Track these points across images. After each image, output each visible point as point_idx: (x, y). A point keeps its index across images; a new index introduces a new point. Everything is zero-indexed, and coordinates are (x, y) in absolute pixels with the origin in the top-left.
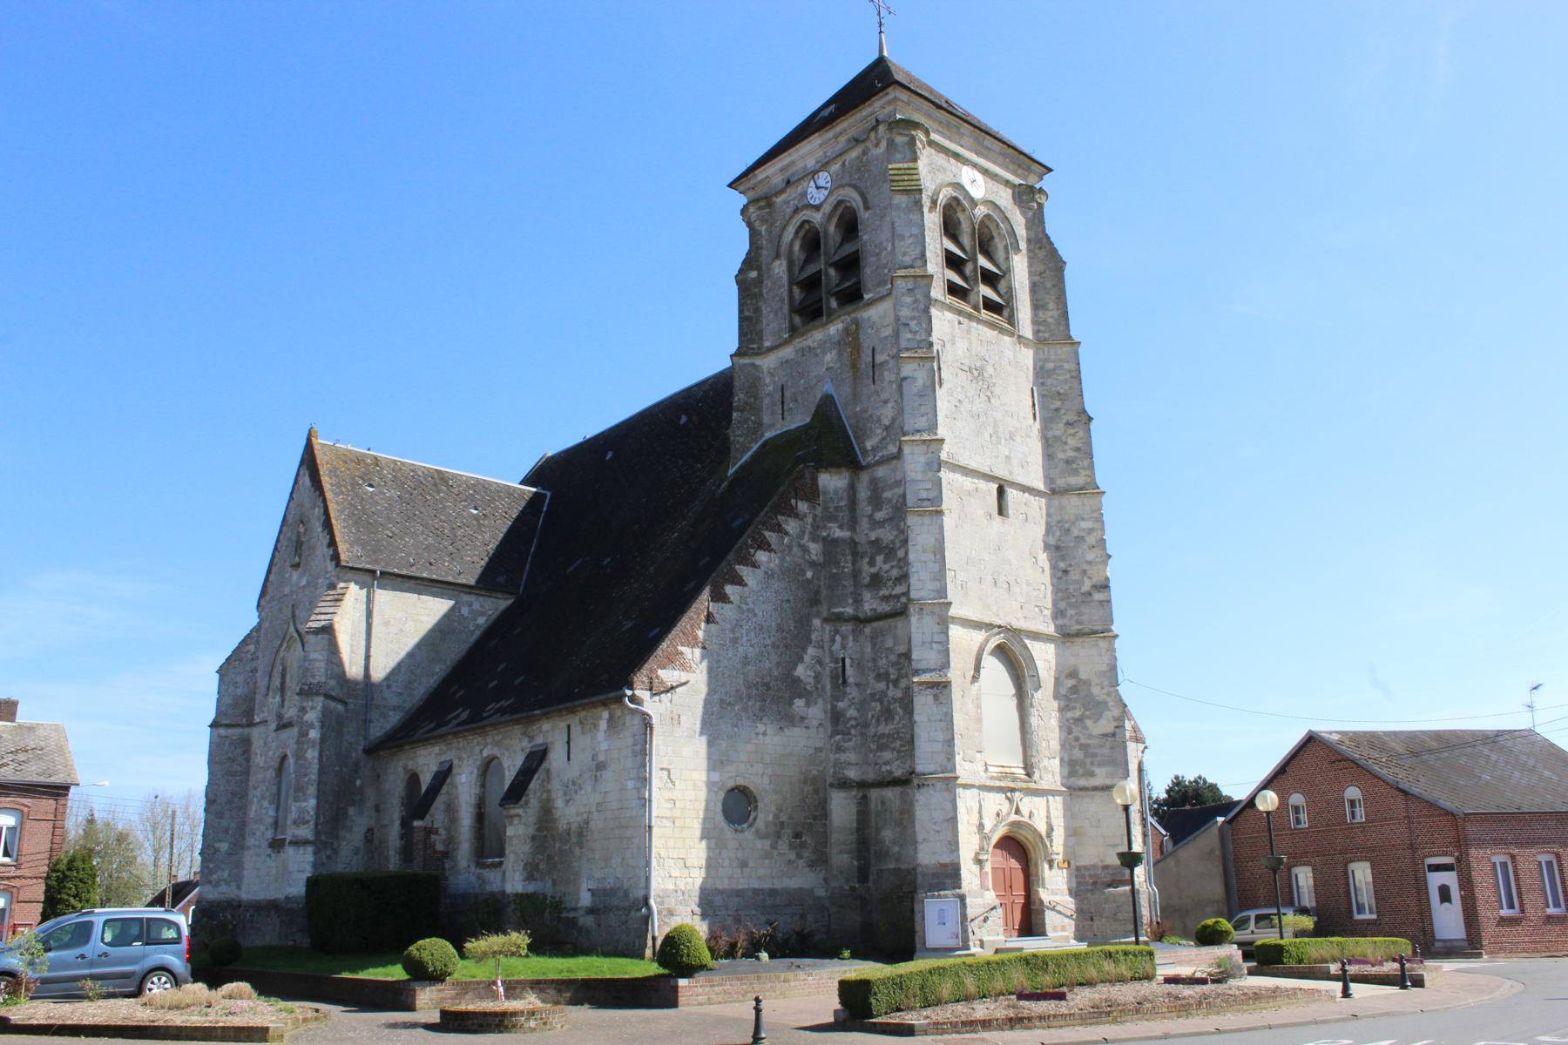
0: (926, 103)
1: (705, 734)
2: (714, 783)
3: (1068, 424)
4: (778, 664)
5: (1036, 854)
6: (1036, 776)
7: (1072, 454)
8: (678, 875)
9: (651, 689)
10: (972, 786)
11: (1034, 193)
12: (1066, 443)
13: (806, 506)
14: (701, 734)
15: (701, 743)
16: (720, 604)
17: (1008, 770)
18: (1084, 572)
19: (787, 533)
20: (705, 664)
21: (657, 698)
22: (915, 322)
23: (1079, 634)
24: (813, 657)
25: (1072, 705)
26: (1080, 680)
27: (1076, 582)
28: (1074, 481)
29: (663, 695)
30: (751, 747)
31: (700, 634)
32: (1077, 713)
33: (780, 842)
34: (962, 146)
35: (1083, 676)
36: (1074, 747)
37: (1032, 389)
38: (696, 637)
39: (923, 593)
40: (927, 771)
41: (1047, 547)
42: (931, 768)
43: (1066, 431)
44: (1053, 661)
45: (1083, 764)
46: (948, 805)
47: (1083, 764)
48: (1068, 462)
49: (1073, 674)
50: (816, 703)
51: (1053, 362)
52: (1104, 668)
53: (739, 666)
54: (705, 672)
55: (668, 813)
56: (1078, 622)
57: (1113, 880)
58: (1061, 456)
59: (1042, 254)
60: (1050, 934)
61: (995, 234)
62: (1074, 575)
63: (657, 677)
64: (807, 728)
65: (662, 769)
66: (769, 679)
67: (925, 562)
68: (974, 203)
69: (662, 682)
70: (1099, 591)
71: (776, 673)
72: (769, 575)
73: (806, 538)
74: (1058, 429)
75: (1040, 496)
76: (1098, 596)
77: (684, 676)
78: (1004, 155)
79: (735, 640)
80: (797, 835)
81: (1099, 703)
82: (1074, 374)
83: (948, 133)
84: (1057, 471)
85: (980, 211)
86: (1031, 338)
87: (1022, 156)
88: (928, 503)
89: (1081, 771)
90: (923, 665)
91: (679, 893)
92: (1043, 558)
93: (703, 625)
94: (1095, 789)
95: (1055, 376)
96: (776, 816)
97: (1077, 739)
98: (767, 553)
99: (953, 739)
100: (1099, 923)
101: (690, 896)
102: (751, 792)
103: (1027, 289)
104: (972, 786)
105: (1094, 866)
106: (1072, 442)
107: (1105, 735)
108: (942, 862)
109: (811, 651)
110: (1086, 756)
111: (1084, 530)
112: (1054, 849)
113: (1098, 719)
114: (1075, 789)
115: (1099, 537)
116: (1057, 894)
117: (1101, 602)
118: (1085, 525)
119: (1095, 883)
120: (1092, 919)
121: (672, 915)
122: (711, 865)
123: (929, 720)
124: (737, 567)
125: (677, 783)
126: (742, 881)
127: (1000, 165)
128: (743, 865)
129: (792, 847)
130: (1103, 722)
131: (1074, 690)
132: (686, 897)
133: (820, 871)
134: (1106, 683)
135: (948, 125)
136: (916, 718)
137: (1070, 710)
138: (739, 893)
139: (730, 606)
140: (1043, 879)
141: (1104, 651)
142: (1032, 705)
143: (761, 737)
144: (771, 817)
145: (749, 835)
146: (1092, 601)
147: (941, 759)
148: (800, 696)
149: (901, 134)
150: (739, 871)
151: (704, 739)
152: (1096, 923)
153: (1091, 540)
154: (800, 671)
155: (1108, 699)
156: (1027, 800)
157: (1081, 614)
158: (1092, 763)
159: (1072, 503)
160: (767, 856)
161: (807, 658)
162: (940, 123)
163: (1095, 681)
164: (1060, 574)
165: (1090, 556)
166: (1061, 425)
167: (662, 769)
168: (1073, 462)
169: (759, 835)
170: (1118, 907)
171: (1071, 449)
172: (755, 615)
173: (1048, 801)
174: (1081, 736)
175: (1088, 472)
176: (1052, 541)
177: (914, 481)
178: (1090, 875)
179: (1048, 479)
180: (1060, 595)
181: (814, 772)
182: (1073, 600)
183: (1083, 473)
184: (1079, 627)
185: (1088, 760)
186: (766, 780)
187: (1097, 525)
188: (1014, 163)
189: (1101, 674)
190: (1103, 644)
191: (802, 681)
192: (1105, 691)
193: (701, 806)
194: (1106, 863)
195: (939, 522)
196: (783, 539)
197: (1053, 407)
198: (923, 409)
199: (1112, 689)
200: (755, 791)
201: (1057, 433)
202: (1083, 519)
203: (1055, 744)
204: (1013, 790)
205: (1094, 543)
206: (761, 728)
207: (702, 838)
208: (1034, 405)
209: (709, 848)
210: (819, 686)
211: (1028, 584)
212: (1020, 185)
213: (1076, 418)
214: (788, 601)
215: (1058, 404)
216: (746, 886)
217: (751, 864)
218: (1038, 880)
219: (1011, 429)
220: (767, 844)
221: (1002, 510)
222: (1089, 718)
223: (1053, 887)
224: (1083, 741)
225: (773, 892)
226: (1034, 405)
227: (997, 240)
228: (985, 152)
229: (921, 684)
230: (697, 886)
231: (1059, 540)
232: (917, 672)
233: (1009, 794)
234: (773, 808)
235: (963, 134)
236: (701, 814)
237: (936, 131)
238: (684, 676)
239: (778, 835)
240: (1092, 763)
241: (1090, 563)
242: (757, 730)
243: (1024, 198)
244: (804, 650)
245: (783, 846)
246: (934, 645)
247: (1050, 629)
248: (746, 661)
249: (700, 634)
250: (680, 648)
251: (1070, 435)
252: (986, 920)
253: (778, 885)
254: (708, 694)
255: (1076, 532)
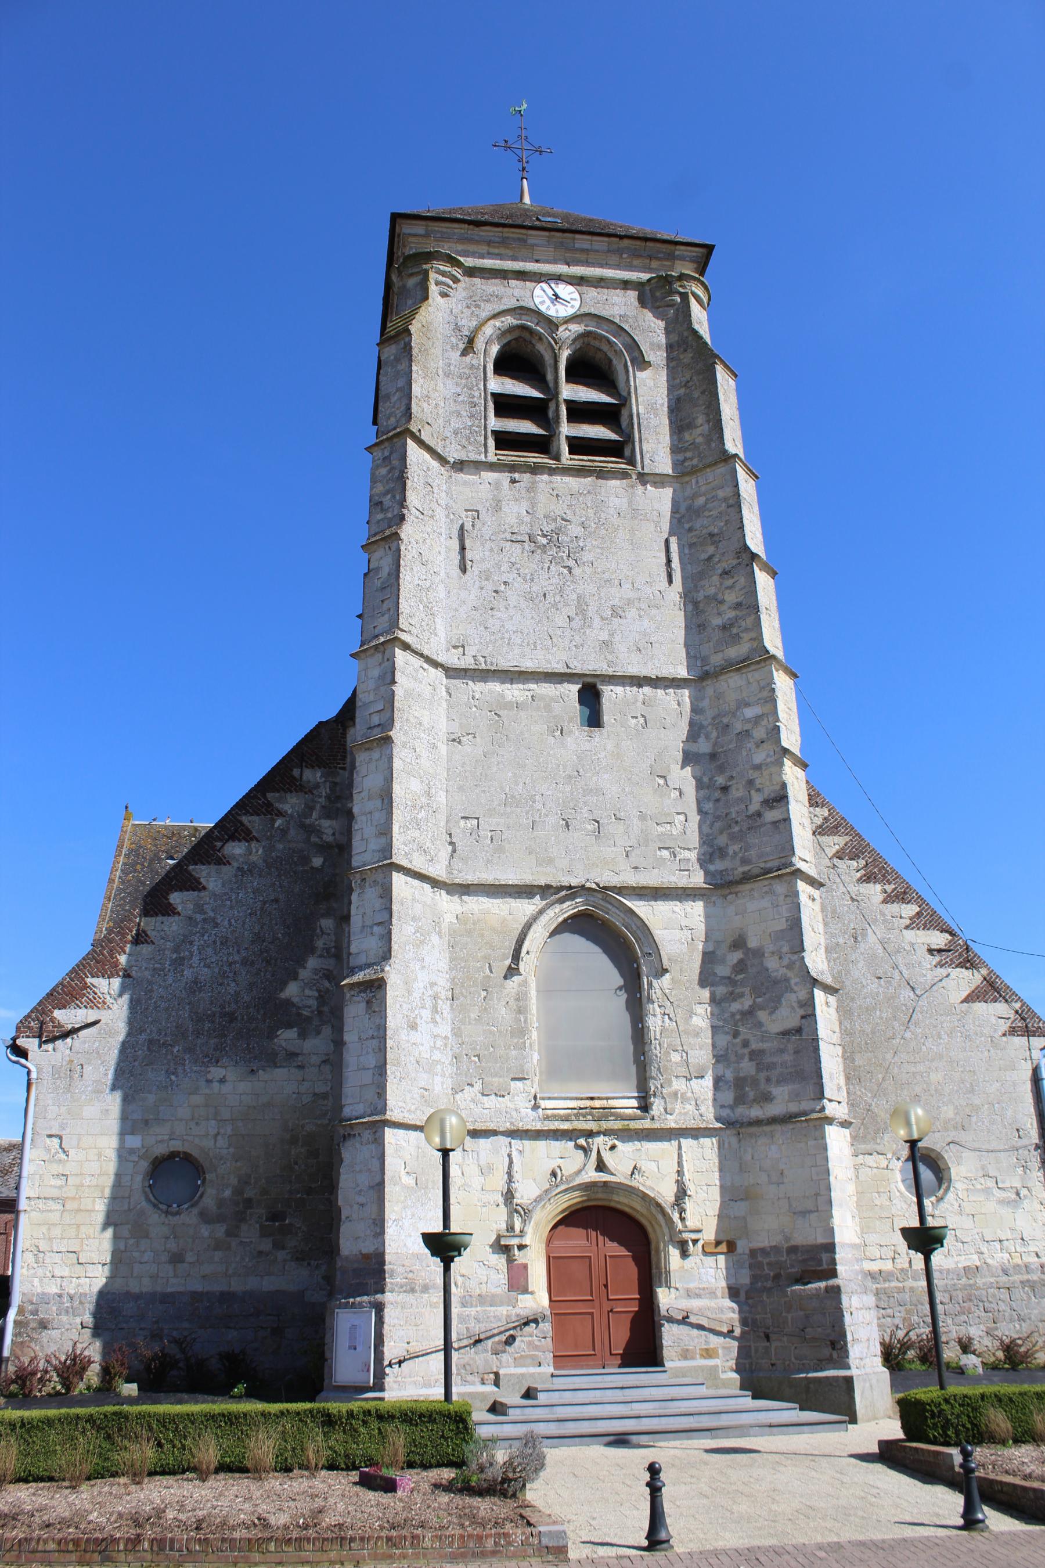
0: (456, 225)
1: (121, 1088)
2: (132, 1151)
3: (726, 573)
4: (251, 986)
5: (658, 1233)
6: (657, 1106)
7: (731, 614)
8: (66, 1273)
9: (40, 1037)
10: (495, 1133)
11: (670, 284)
12: (722, 602)
13: (319, 774)
14: (114, 1088)
15: (114, 1102)
16: (160, 918)
17: (597, 1104)
18: (751, 782)
19: (280, 814)
20: (126, 997)
21: (50, 1047)
22: (389, 496)
23: (747, 878)
24: (316, 971)
25: (738, 990)
26: (748, 951)
27: (740, 800)
28: (734, 652)
29: (59, 1043)
30: (197, 1099)
31: (123, 959)
32: (747, 1003)
33: (244, 1227)
34: (537, 261)
35: (753, 943)
36: (742, 1057)
37: (667, 542)
38: (116, 964)
39: (367, 857)
40: (355, 1114)
41: (688, 758)
42: (360, 1109)
43: (721, 584)
44: (702, 927)
45: (755, 1082)
46: (376, 1163)
47: (755, 1082)
48: (724, 628)
49: (739, 943)
50: (318, 1033)
51: (704, 495)
52: (782, 925)
53: (184, 994)
54: (126, 1007)
55: (55, 1193)
56: (744, 861)
57: (804, 1272)
58: (717, 621)
59: (687, 358)
60: (668, 1364)
61: (611, 355)
62: (737, 792)
63: (53, 1020)
64: (301, 1067)
65: (50, 1136)
66: (234, 1006)
67: (370, 813)
68: (552, 324)
69: (60, 1026)
70: (772, 808)
71: (247, 998)
72: (246, 871)
73: (315, 815)
74: (711, 586)
75: (678, 687)
76: (771, 816)
77: (91, 1015)
78: (619, 252)
79: (179, 962)
80: (274, 1217)
81: (776, 982)
82: (731, 502)
83: (510, 253)
84: (711, 644)
85: (568, 333)
86: (670, 472)
87: (649, 244)
88: (379, 729)
89: (751, 1095)
90: (362, 960)
91: (65, 1299)
92: (684, 778)
93: (128, 948)
94: (773, 1121)
95: (706, 514)
96: (238, 1191)
97: (746, 1044)
98: (244, 845)
99: (385, 1063)
100: (778, 1344)
101: (81, 1303)
102: (196, 1159)
103: (666, 409)
104: (495, 1133)
105: (776, 1249)
106: (731, 598)
107: (785, 1033)
108: (364, 1251)
109: (312, 963)
110: (759, 1070)
111: (749, 721)
112: (690, 1223)
113: (776, 1008)
114: (742, 1125)
115: (771, 726)
116: (698, 1296)
117: (775, 823)
118: (749, 712)
119: (777, 1277)
120: (767, 1337)
121: (45, 1328)
122: (119, 1260)
123: (360, 1039)
124: (191, 867)
125: (72, 1152)
126: (173, 1281)
127: (618, 267)
128: (177, 1259)
129: (264, 1232)
130: (783, 1012)
131: (740, 967)
132: (76, 1303)
133: (317, 1267)
134: (785, 949)
135: (504, 242)
136: (347, 1037)
137: (734, 1000)
138: (166, 1298)
139: (176, 918)
140: (668, 1273)
141: (782, 898)
142: (650, 1000)
143: (216, 1085)
144: (228, 1193)
145: (189, 1218)
146: (763, 825)
147: (370, 1094)
148: (289, 1026)
149: (412, 275)
150: (170, 1268)
151: (118, 1096)
152: (775, 1344)
153: (759, 733)
154: (292, 990)
155: (790, 974)
156: (625, 1148)
157: (747, 848)
158: (768, 1080)
159: (733, 684)
160: (218, 1246)
161: (304, 974)
162: (489, 243)
163: (769, 948)
164: (717, 794)
165: (759, 758)
166: (716, 579)
167: (50, 1136)
168: (732, 625)
169: (205, 1217)
170: (807, 1317)
171: (730, 608)
172: (216, 925)
173: (680, 1147)
174: (752, 1039)
175: (753, 635)
176: (704, 746)
177: (366, 705)
178: (769, 1264)
179: (693, 657)
180: (718, 825)
181: (308, 1128)
182: (736, 829)
183: (746, 636)
184: (746, 868)
185: (762, 1076)
186: (221, 1142)
187: (767, 708)
188: (640, 256)
189: (778, 936)
190: (780, 888)
191: (293, 1005)
192: (786, 962)
193: (108, 1181)
194: (793, 1243)
195: (388, 752)
196: (273, 821)
197: (704, 556)
198: (385, 605)
199: (795, 957)
200: (201, 1161)
201: (712, 591)
202: (747, 705)
203: (702, 1054)
204: (590, 1134)
205: (765, 736)
206: (216, 1072)
207: (106, 1225)
208: (669, 561)
209: (116, 1237)
210: (326, 1009)
211: (642, 817)
212: (649, 280)
213: (735, 562)
214: (276, 901)
215: (711, 550)
216: (181, 1289)
217: (190, 1257)
218: (660, 1273)
219: (616, 602)
220: (220, 1230)
221: (594, 720)
222: (762, 1008)
223: (692, 1285)
224: (754, 1046)
225: (226, 1297)
226: (669, 561)
227: (615, 362)
228: (583, 257)
229: (352, 986)
230: (96, 1289)
231: (715, 745)
232: (352, 971)
233: (582, 1141)
234: (234, 1181)
235: (533, 246)
236: (107, 1192)
237: (466, 254)
238: (91, 1015)
239: (240, 1217)
240: (768, 1080)
241: (758, 767)
242: (209, 1076)
243: (658, 294)
244: (301, 963)
245: (250, 1232)
246: (375, 928)
247: (698, 879)
248: (195, 986)
249: (123, 959)
250: (89, 980)
251: (727, 588)
252: (510, 1341)
253: (237, 1286)
254: (129, 1034)
255: (738, 727)
